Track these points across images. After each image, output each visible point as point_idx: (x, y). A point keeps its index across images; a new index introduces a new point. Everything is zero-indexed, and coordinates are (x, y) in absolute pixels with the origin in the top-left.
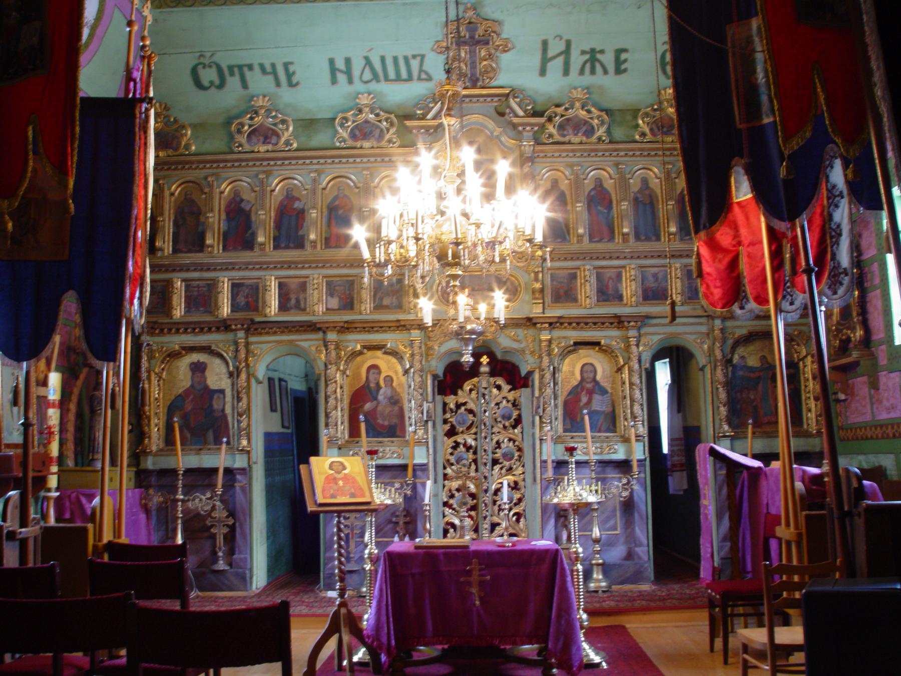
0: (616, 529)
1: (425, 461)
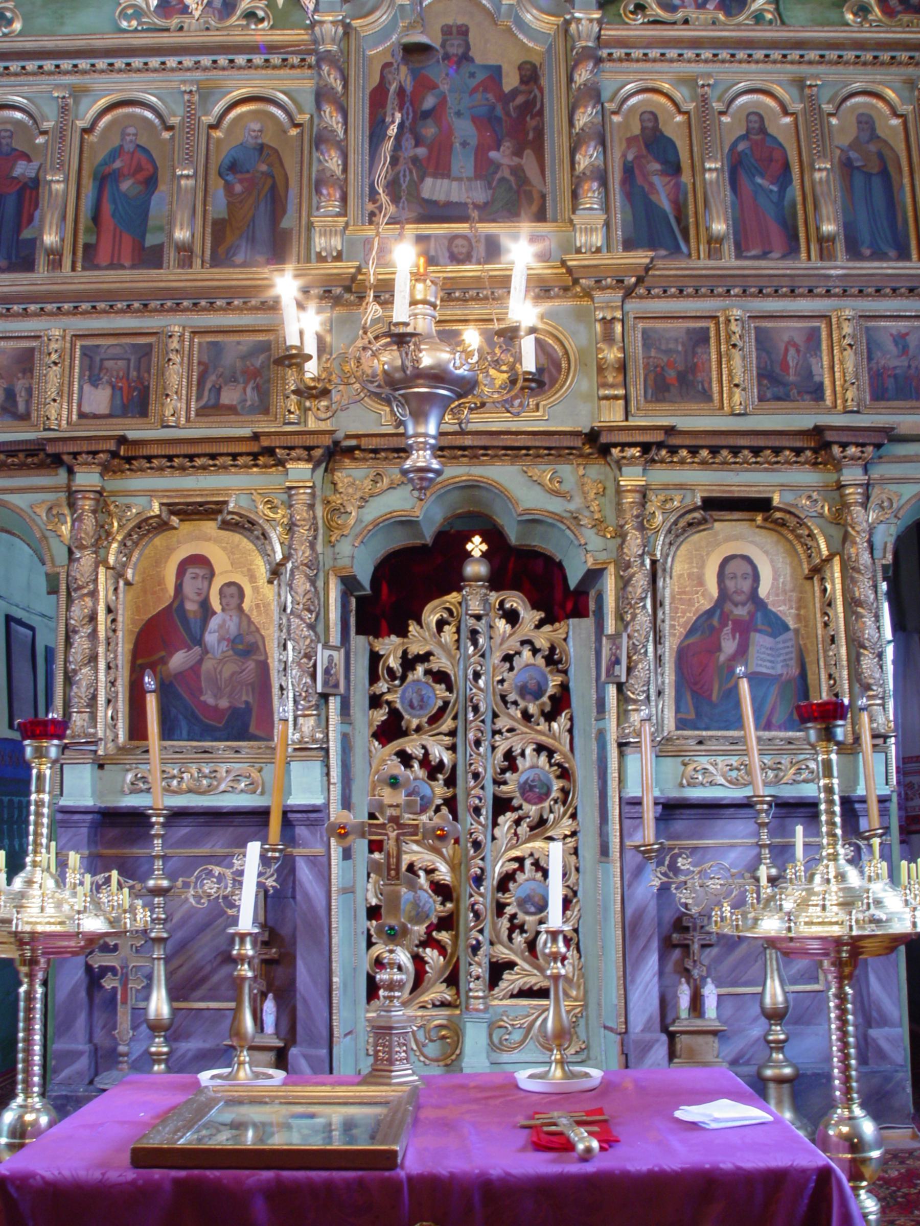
1: (319, 801)
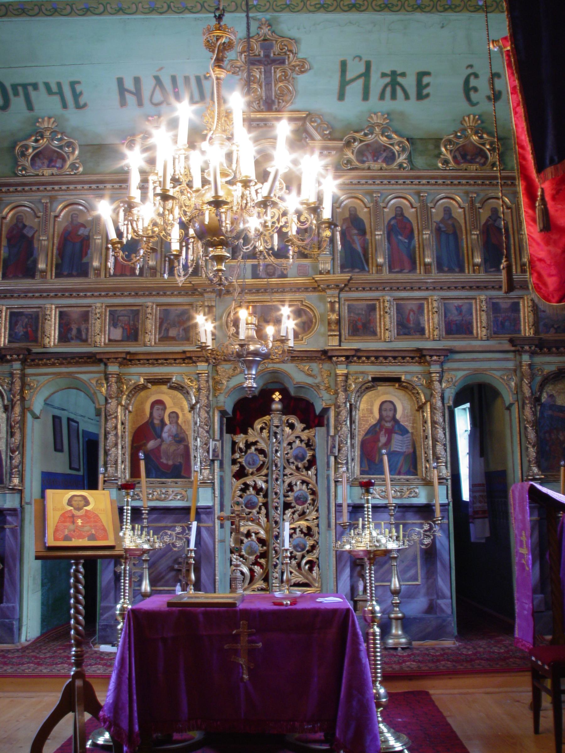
0: (416, 580)
1: (210, 504)
